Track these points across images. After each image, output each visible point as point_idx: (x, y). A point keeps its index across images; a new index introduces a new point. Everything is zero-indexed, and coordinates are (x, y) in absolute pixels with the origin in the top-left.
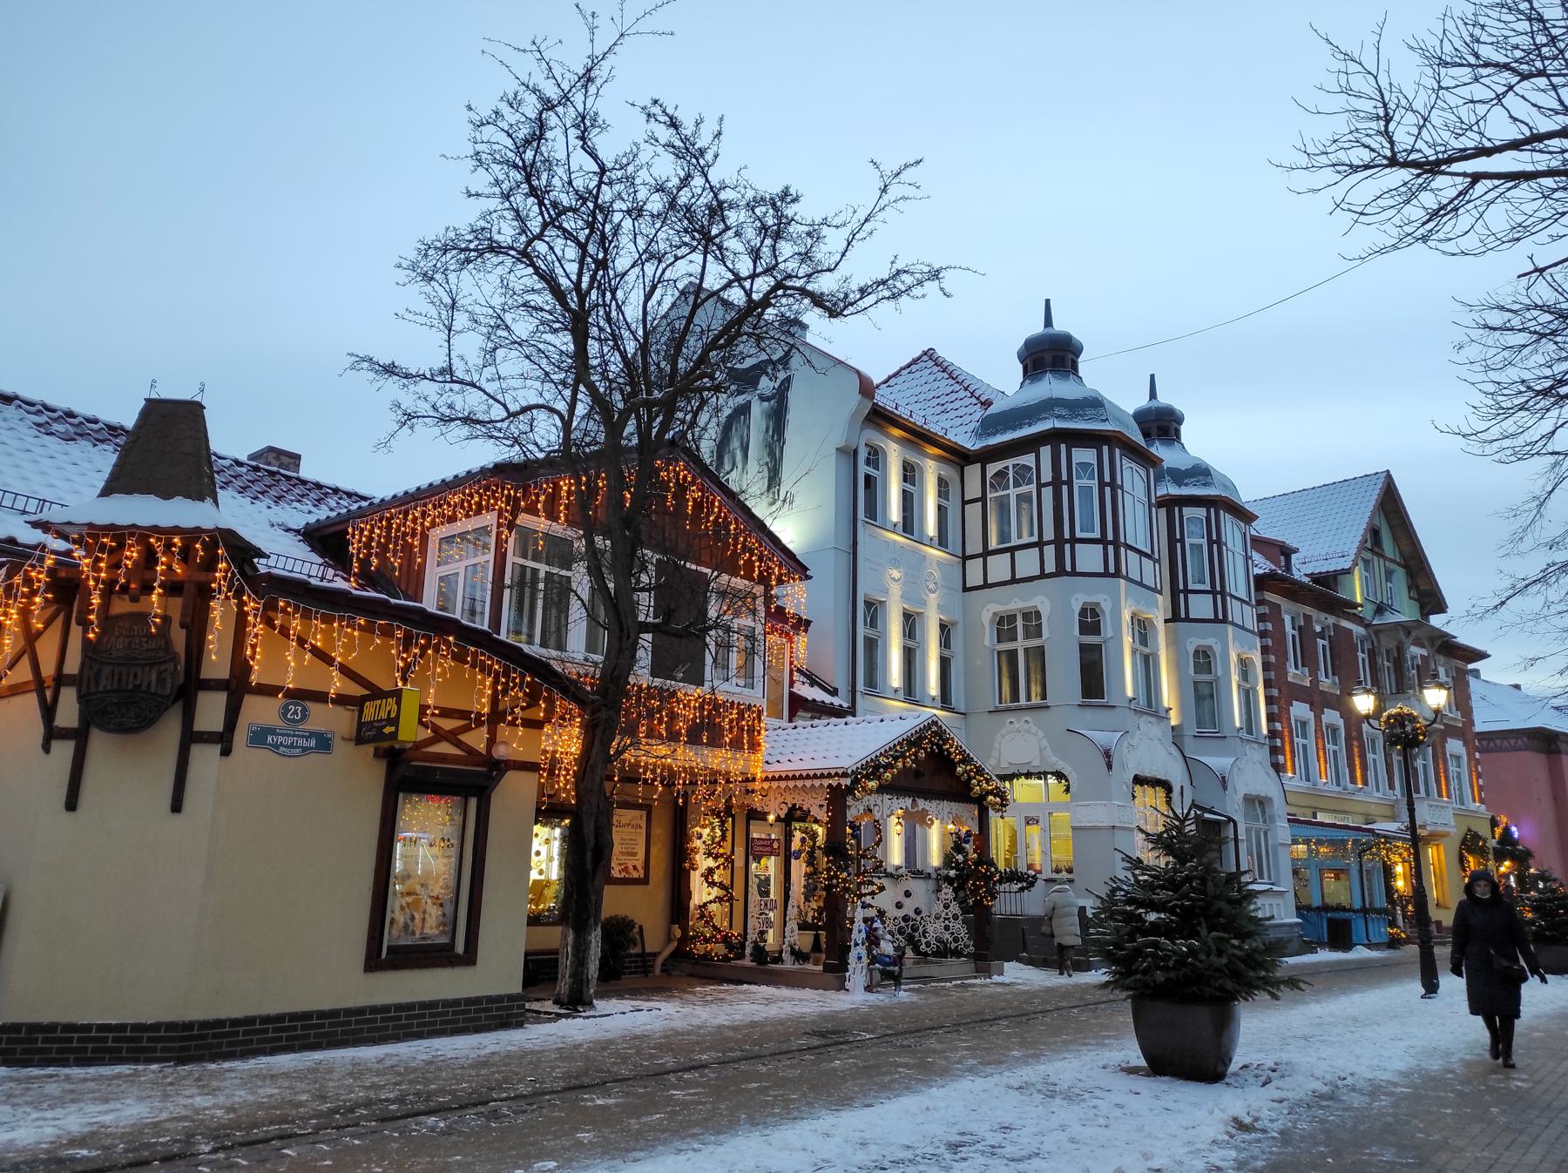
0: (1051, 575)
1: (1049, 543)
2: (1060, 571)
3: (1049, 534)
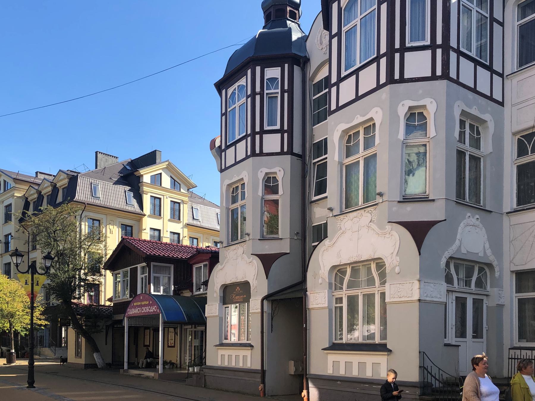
0: (258, 155)
1: (439, 46)
2: (445, 75)
3: (439, 41)
